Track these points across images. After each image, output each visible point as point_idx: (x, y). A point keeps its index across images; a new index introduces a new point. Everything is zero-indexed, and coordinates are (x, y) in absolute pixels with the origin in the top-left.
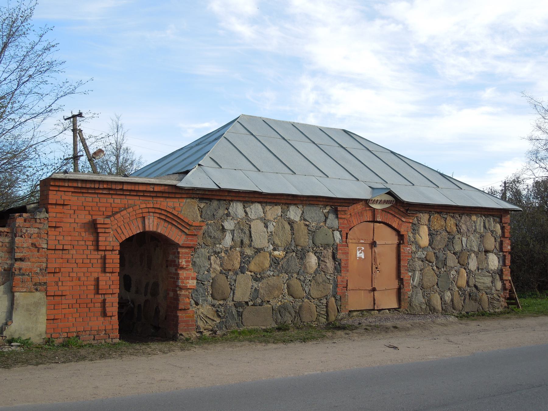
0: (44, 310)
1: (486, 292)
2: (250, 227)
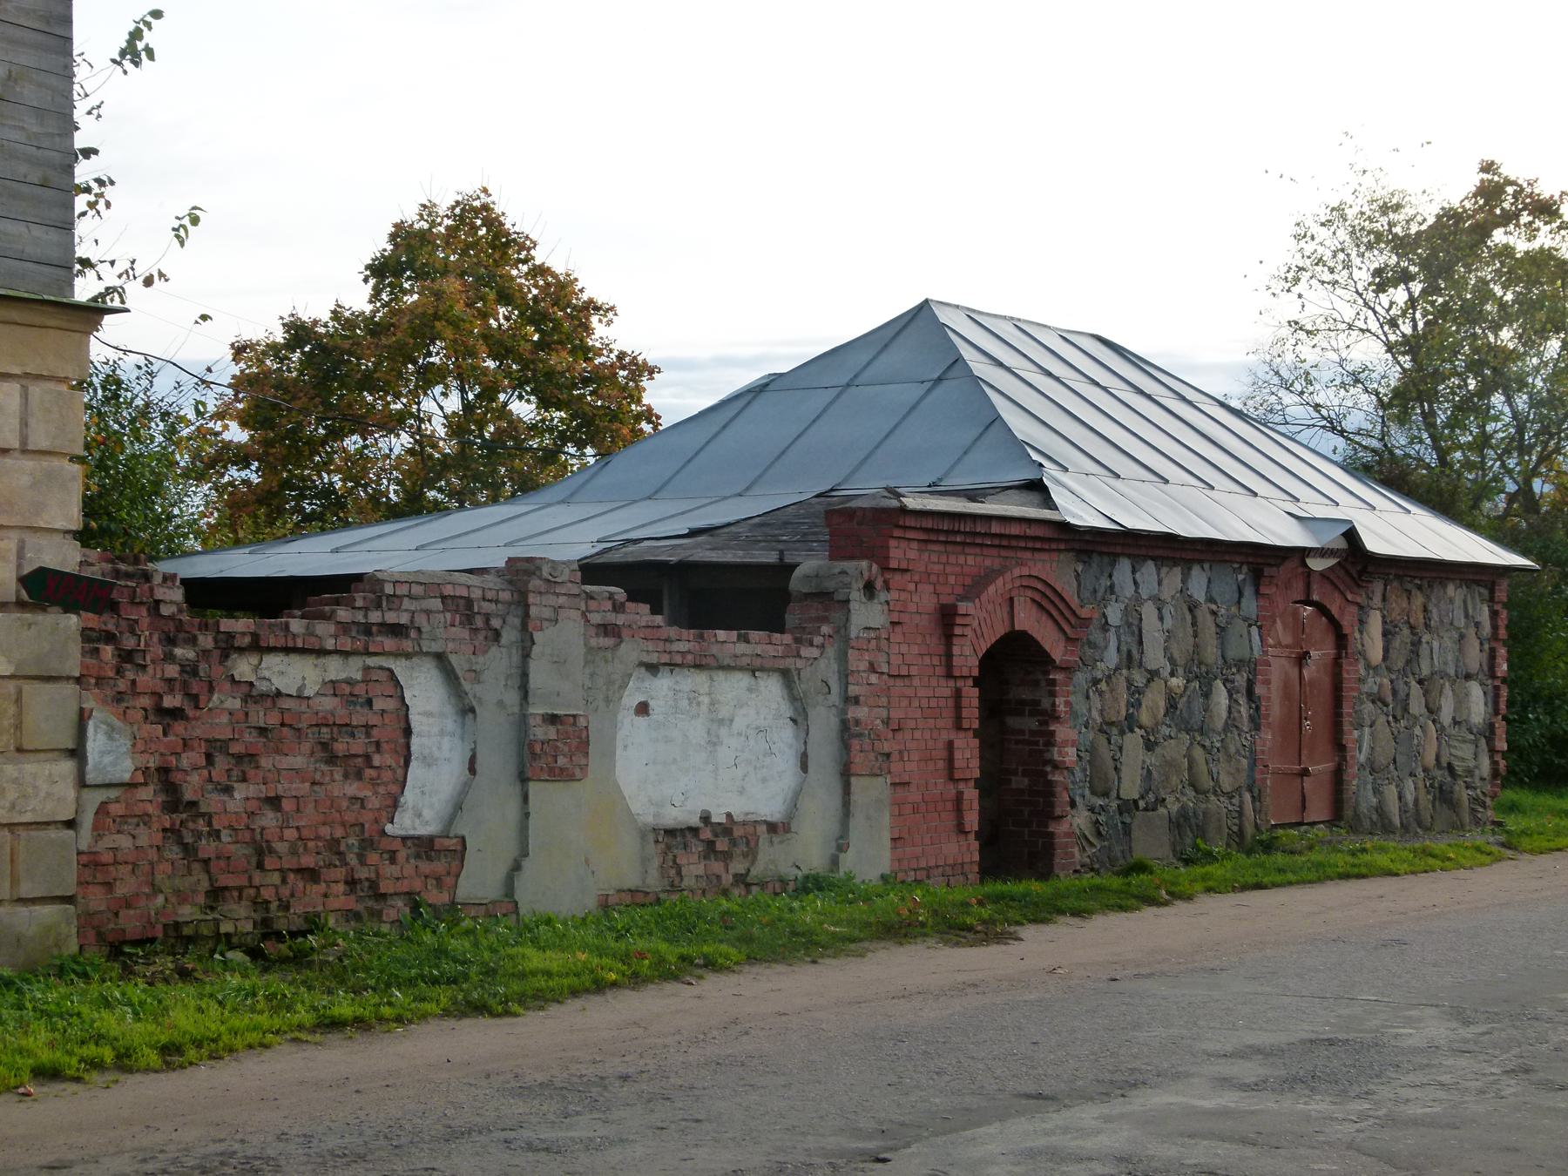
2: (1141, 619)
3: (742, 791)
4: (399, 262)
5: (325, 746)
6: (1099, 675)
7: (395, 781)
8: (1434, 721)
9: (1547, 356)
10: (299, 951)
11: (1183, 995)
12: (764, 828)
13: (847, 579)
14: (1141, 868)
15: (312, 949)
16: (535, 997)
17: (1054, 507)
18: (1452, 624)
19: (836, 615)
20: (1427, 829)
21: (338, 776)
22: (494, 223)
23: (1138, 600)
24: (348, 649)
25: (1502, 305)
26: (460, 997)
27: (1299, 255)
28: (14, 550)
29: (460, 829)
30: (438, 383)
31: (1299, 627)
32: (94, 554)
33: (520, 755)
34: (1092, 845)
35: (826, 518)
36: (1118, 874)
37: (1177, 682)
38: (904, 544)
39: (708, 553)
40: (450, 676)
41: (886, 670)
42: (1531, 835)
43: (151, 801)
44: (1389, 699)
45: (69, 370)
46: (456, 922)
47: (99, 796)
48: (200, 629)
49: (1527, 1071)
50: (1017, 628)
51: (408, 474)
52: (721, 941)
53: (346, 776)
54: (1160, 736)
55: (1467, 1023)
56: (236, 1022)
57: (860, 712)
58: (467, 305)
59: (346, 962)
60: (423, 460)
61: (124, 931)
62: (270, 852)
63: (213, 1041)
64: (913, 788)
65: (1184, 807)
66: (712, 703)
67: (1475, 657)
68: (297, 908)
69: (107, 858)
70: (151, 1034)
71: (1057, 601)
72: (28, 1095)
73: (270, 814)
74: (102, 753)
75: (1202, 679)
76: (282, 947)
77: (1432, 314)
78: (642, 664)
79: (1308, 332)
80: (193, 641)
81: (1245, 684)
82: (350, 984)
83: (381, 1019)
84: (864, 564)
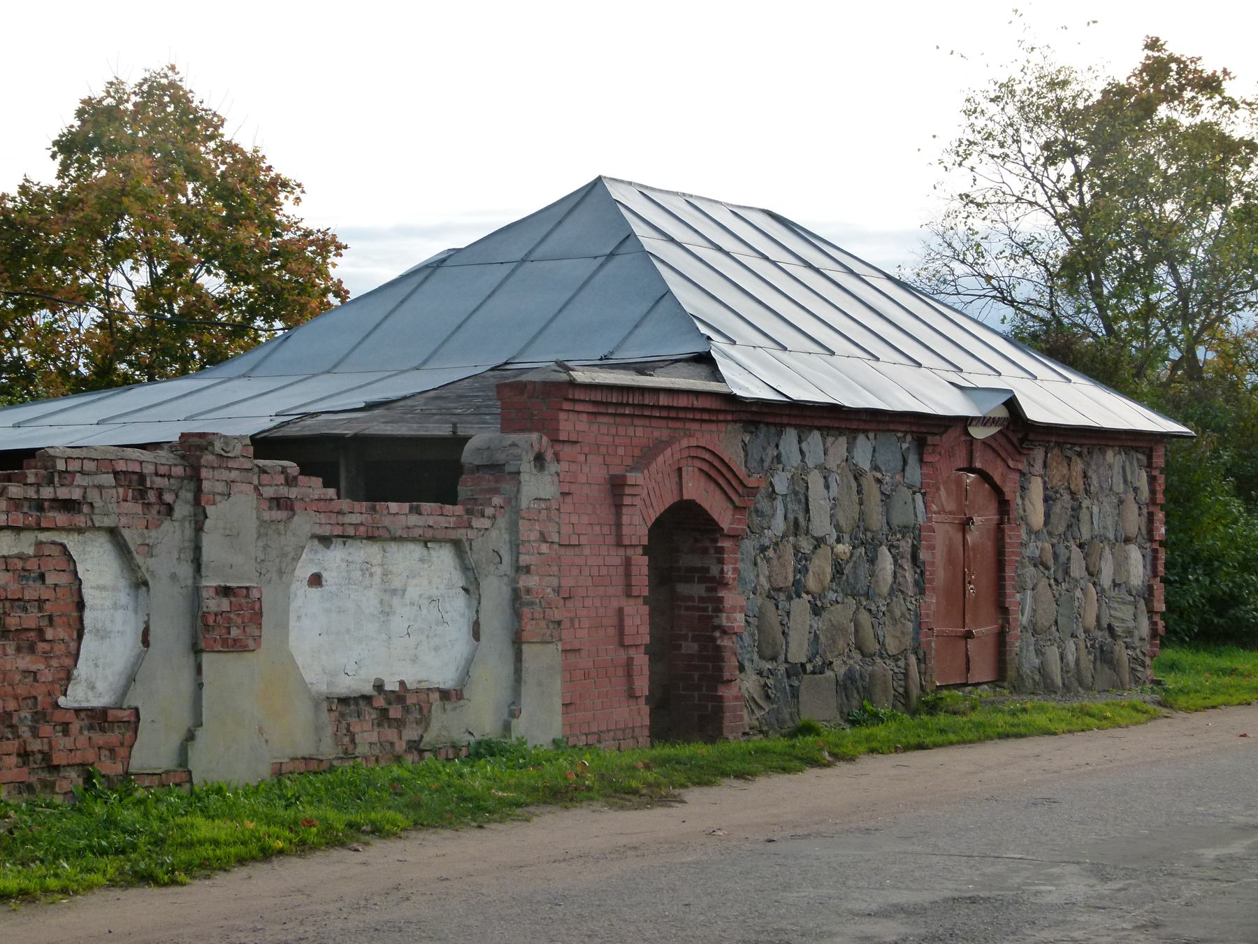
0: (558, 685)
1: (1125, 642)
2: (807, 488)
3: (415, 660)
4: (86, 138)
7: (68, 654)
8: (1094, 584)
9: (1208, 230)
12: (437, 695)
13: (516, 451)
14: (807, 729)
16: (202, 866)
17: (720, 379)
18: (1111, 489)
19: (507, 486)
20: (1089, 689)
22: (181, 99)
23: (804, 469)
24: (21, 525)
25: (1167, 179)
26: (127, 867)
27: (969, 130)
29: (132, 701)
30: (127, 258)
31: (962, 493)
33: (194, 627)
34: (761, 708)
36: (784, 736)
37: (843, 549)
38: (572, 416)
39: (383, 426)
40: (123, 549)
41: (557, 540)
42: (1188, 693)
44: (1051, 563)
46: (129, 793)
49: (1157, 926)
50: (685, 497)
51: (98, 347)
52: (389, 808)
53: (19, 650)
55: (1105, 879)
57: (530, 581)
58: (155, 181)
59: (16, 834)
60: (112, 333)
65: (850, 670)
66: (385, 574)
67: (1134, 521)
71: (724, 470)
75: (868, 545)
77: (1099, 186)
78: (314, 536)
79: (978, 205)
81: (910, 550)
83: (46, 891)
84: (534, 436)
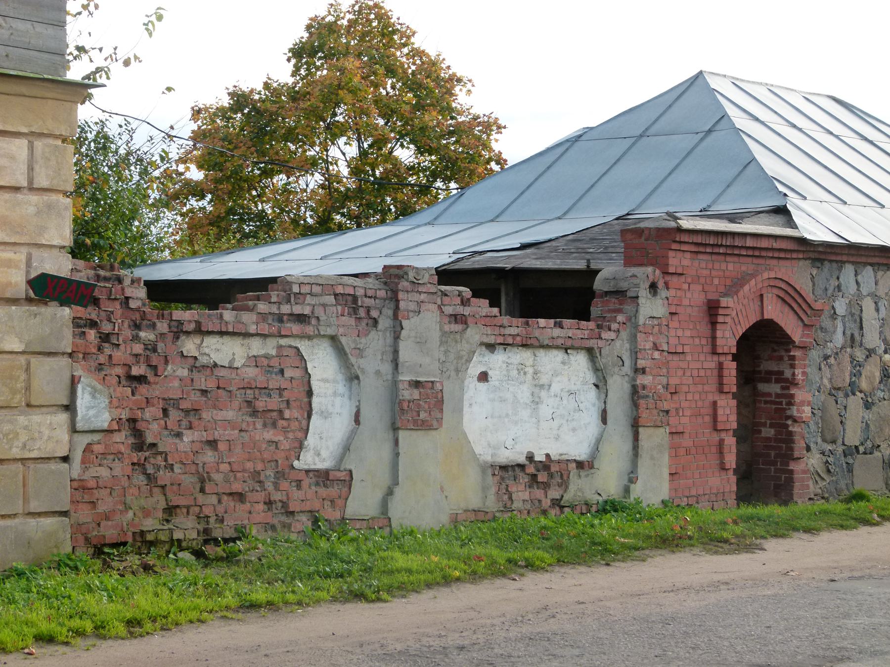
0: (666, 459)
2: (861, 310)
3: (557, 438)
4: (313, 47)
5: (249, 403)
6: (829, 352)
10: (230, 553)
11: (885, 593)
12: (574, 465)
13: (635, 281)
14: (859, 497)
15: (240, 551)
16: (399, 588)
17: (794, 226)
19: (628, 308)
21: (259, 426)
23: (859, 296)
26: (345, 587)
28: (24, 261)
29: (348, 465)
30: (342, 136)
32: (81, 263)
33: (393, 410)
34: (823, 479)
35: (622, 236)
38: (679, 254)
39: (534, 262)
40: (340, 352)
41: (666, 348)
43: (123, 443)
45: (64, 131)
47: (86, 439)
48: (158, 318)
50: (766, 317)
51: (320, 202)
52: (539, 549)
53: (265, 425)
54: (875, 398)
56: (181, 604)
58: (363, 78)
59: (264, 561)
61: (104, 537)
62: (210, 480)
63: (165, 617)
64: (686, 436)
66: (535, 373)
68: (229, 522)
69: (92, 484)
70: (119, 612)
72: (30, 654)
73: (210, 453)
74: (89, 408)
76: (219, 549)
78: (482, 344)
80: (153, 326)
82: (266, 577)
83: (286, 603)
84: (650, 269)
